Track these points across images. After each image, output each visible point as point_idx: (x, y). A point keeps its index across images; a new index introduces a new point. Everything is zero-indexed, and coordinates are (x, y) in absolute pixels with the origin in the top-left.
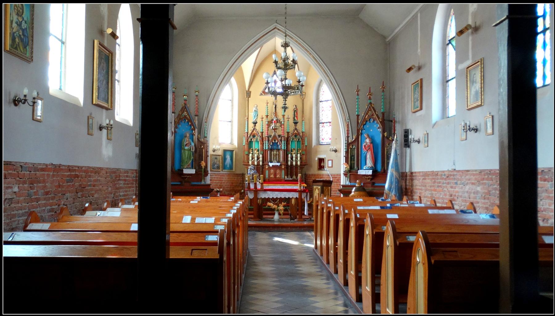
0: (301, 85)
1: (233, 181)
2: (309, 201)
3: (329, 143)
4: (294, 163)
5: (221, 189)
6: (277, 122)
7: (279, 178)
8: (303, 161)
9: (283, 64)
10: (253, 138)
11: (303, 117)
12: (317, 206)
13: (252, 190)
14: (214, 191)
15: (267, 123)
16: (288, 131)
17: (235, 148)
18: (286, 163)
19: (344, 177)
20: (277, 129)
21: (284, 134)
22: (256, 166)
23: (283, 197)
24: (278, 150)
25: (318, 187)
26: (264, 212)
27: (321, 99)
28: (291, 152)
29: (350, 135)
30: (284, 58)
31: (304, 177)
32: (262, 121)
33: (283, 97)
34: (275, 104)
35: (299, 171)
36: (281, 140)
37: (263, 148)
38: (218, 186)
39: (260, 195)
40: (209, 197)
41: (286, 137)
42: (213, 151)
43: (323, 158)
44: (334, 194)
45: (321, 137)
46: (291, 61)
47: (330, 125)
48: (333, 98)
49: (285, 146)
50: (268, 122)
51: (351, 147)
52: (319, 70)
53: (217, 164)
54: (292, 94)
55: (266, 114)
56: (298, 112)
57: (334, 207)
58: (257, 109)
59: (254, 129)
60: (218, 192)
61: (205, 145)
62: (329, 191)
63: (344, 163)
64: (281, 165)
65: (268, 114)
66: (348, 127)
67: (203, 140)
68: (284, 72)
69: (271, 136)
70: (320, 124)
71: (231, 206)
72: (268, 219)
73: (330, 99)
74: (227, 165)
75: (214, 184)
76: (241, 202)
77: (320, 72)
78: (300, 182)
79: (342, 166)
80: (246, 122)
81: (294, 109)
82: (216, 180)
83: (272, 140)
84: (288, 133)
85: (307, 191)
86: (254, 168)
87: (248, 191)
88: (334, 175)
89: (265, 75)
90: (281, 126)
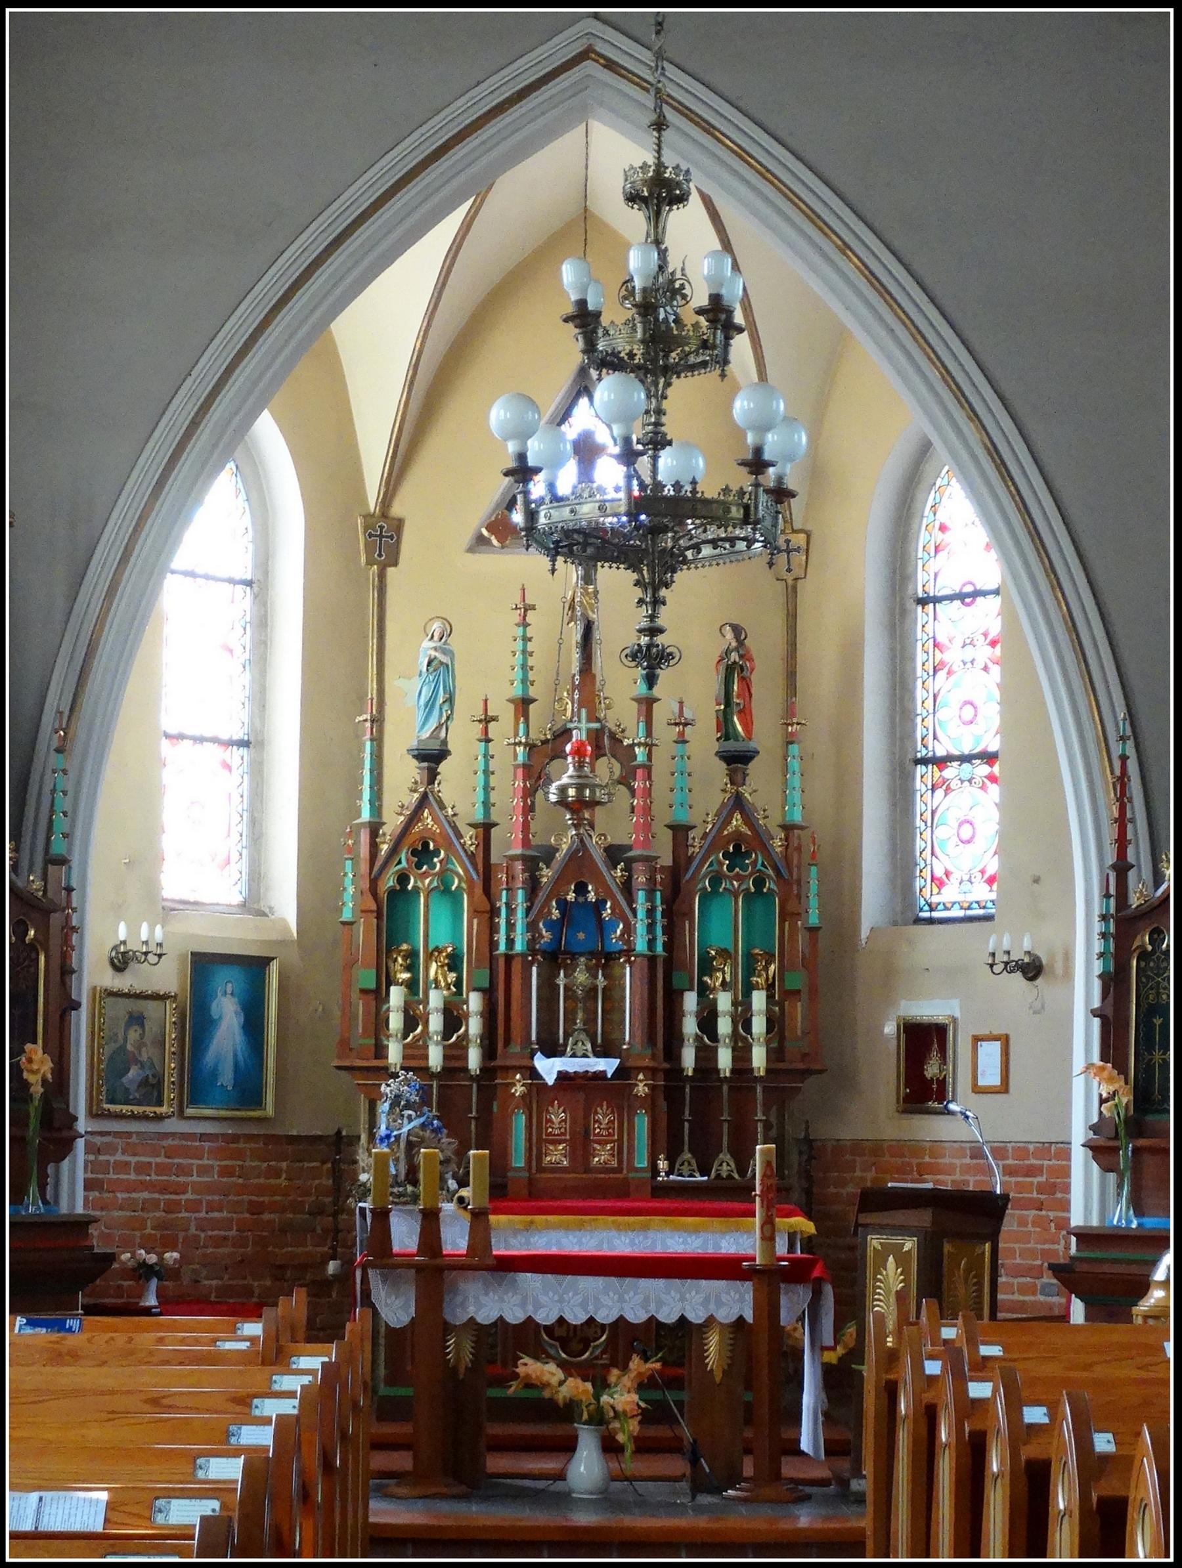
0: (767, 491)
1: (260, 1190)
2: (833, 1349)
3: (981, 912)
4: (724, 1059)
5: (172, 1256)
6: (599, 752)
7: (614, 1170)
8: (788, 1044)
9: (639, 335)
10: (418, 866)
11: (790, 712)
12: (891, 1392)
13: (405, 1262)
14: (115, 1266)
15: (520, 759)
16: (682, 817)
17: (282, 943)
18: (661, 1054)
19: (1095, 1167)
20: (593, 804)
21: (646, 844)
22: (433, 1076)
23: (637, 1316)
24: (606, 960)
25: (896, 1240)
26: (496, 1429)
27: (923, 581)
28: (702, 973)
29: (1138, 852)
30: (644, 290)
31: (794, 1158)
32: (488, 741)
33: (635, 576)
34: (585, 616)
35: (760, 1116)
36: (627, 889)
37: (493, 945)
38: (148, 1231)
39: (463, 1305)
40: (73, 1323)
41: (666, 860)
42: (112, 963)
43: (941, 1020)
44: (1017, 1297)
45: (931, 864)
46: (700, 311)
47: (992, 778)
48: (1015, 577)
49: (659, 930)
50: (531, 747)
51: (1143, 946)
52: (910, 371)
53: (142, 1067)
54: (707, 551)
55: (517, 691)
56: (754, 678)
57: (1014, 1407)
58: (445, 652)
59: (424, 797)
60: (144, 1272)
61: (56, 919)
62: (980, 1276)
63: (1089, 1066)
64: (620, 1072)
65: (532, 692)
66: (1123, 799)
67: (38, 884)
68: (643, 396)
69: (548, 854)
70: (921, 769)
71: (242, 1391)
72: (527, 1483)
73: (994, 586)
74: (214, 1074)
75: (116, 1214)
76: (311, 1362)
77: (917, 380)
78: (768, 1206)
79: (1078, 1085)
80: (361, 750)
81: (728, 652)
82: (130, 1187)
83: (560, 881)
84: (680, 831)
85: (816, 1273)
86: (425, 1093)
87: (370, 1272)
88: (1022, 1151)
89: (498, 415)
90: (625, 780)
